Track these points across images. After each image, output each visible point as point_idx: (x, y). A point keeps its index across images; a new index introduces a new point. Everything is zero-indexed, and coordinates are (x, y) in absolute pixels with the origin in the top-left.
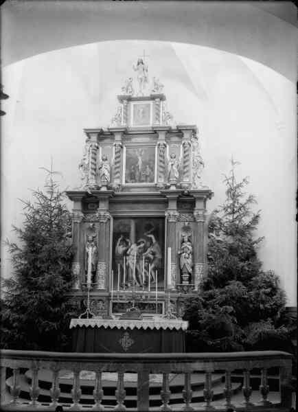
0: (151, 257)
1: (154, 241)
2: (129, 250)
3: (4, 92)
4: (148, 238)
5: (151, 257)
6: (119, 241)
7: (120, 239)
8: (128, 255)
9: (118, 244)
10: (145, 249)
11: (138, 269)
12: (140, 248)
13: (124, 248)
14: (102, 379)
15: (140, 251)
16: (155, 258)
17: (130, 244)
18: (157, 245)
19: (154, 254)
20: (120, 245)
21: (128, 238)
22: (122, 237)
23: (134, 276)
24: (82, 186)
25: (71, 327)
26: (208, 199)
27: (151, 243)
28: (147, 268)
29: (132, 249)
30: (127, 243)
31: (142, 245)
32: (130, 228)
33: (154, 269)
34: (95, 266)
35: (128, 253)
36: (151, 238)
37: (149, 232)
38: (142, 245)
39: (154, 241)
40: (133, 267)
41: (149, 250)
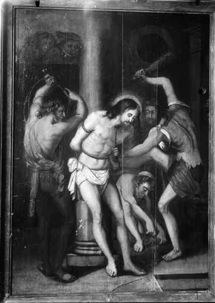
0: (163, 159)
1: (172, 101)
2: (80, 133)
4: (151, 86)
5: (163, 159)
6: (37, 100)
7: (41, 92)
8: (76, 154)
9: (34, 111)
10: (139, 131)
11: (115, 206)
12: (118, 128)
13: (61, 127)
15: (121, 138)
17: (80, 110)
18: (181, 115)
19: (171, 149)
20: (41, 115)
21: (77, 91)
23: (99, 236)
24: (99, 277)
27: (164, 113)
30: (71, 108)
31: (128, 116)
32: (79, 53)
33: (174, 206)
34: (123, 294)
35: (75, 143)
37: (155, 65)
38: (128, 116)
39: (172, 101)
41: (153, 135)
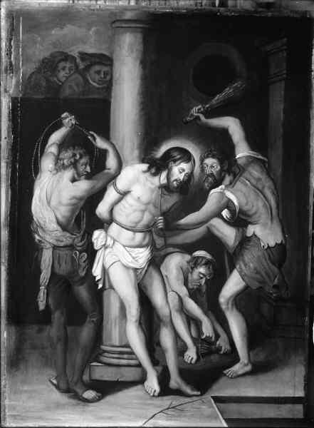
1: (242, 152)
2: (111, 195)
3: (237, 120)
5: (229, 234)
6: (52, 149)
7: (56, 137)
8: (103, 224)
13: (83, 186)
14: (240, 162)
16: (244, 241)
17: (111, 162)
18: (255, 172)
19: (240, 220)
22: (69, 120)
25: (99, 288)
26: (98, 237)
28: (207, 295)
29: (124, 194)
30: (97, 162)
31: (179, 171)
35: (102, 209)
36: (224, 133)
39: (242, 152)
40: (124, 288)
